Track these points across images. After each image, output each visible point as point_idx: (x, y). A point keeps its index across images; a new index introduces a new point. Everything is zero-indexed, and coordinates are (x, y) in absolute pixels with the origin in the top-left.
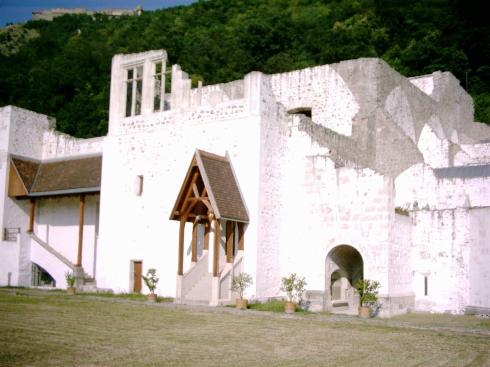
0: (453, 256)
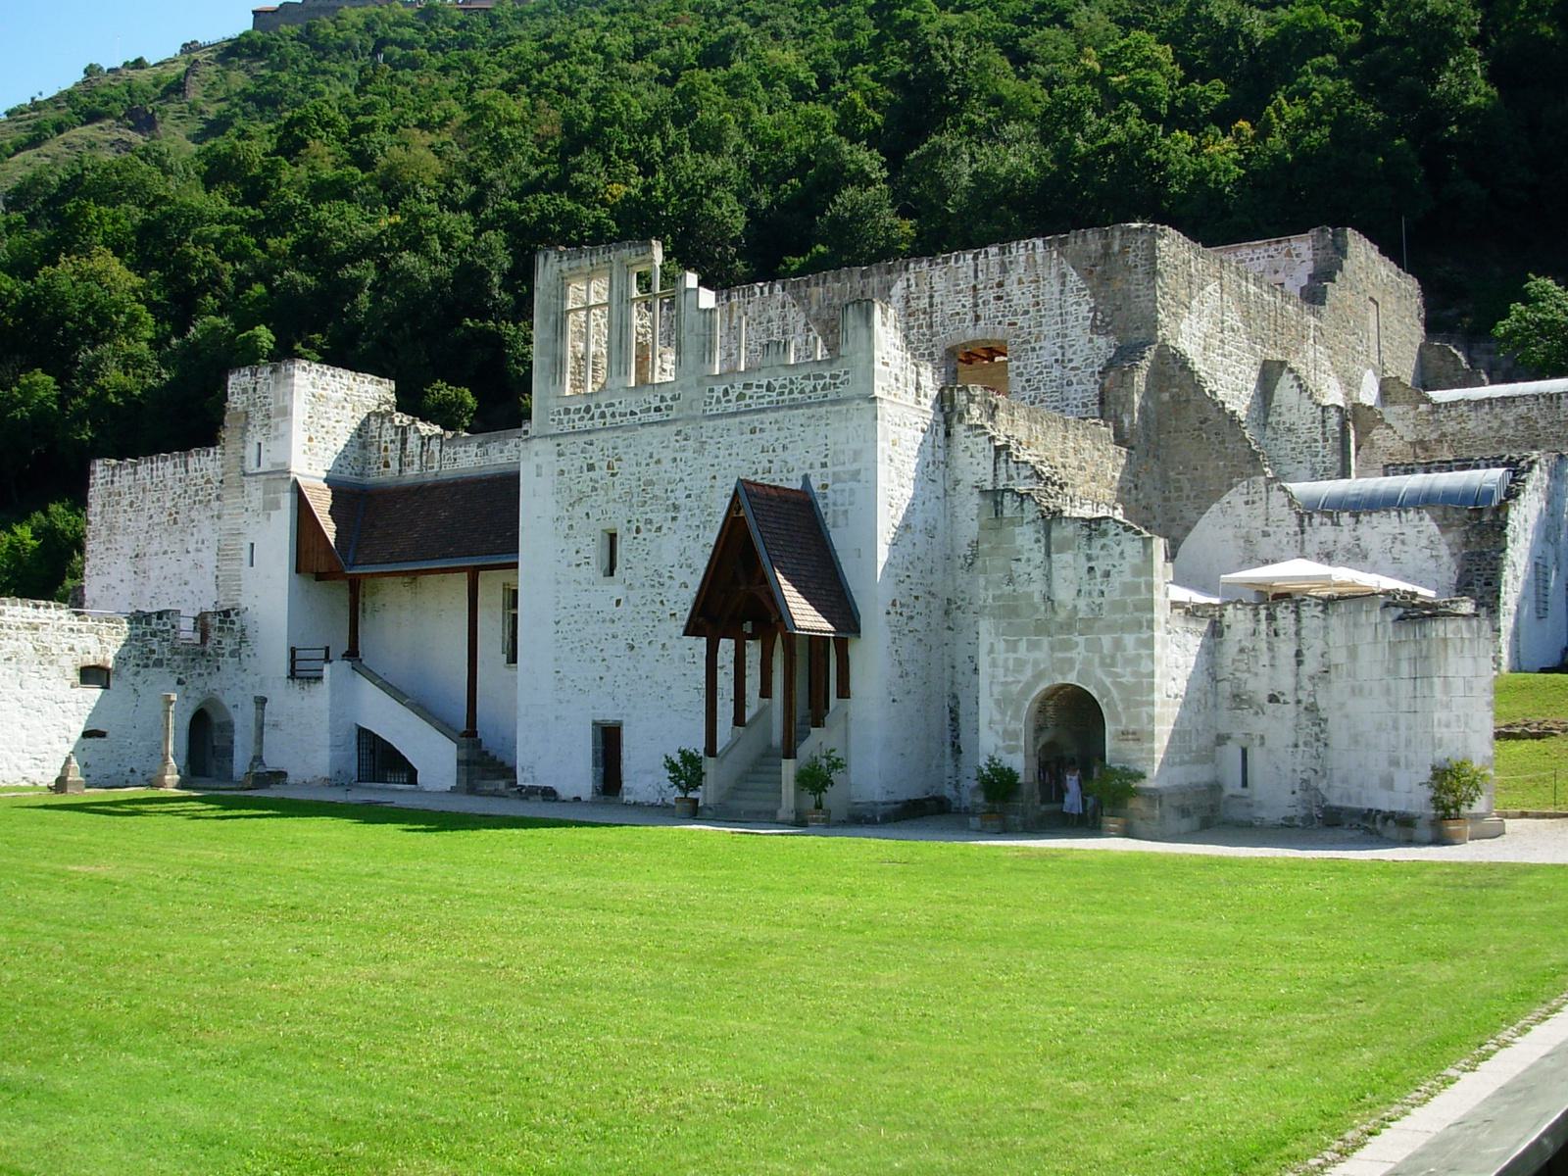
0: (1299, 702)
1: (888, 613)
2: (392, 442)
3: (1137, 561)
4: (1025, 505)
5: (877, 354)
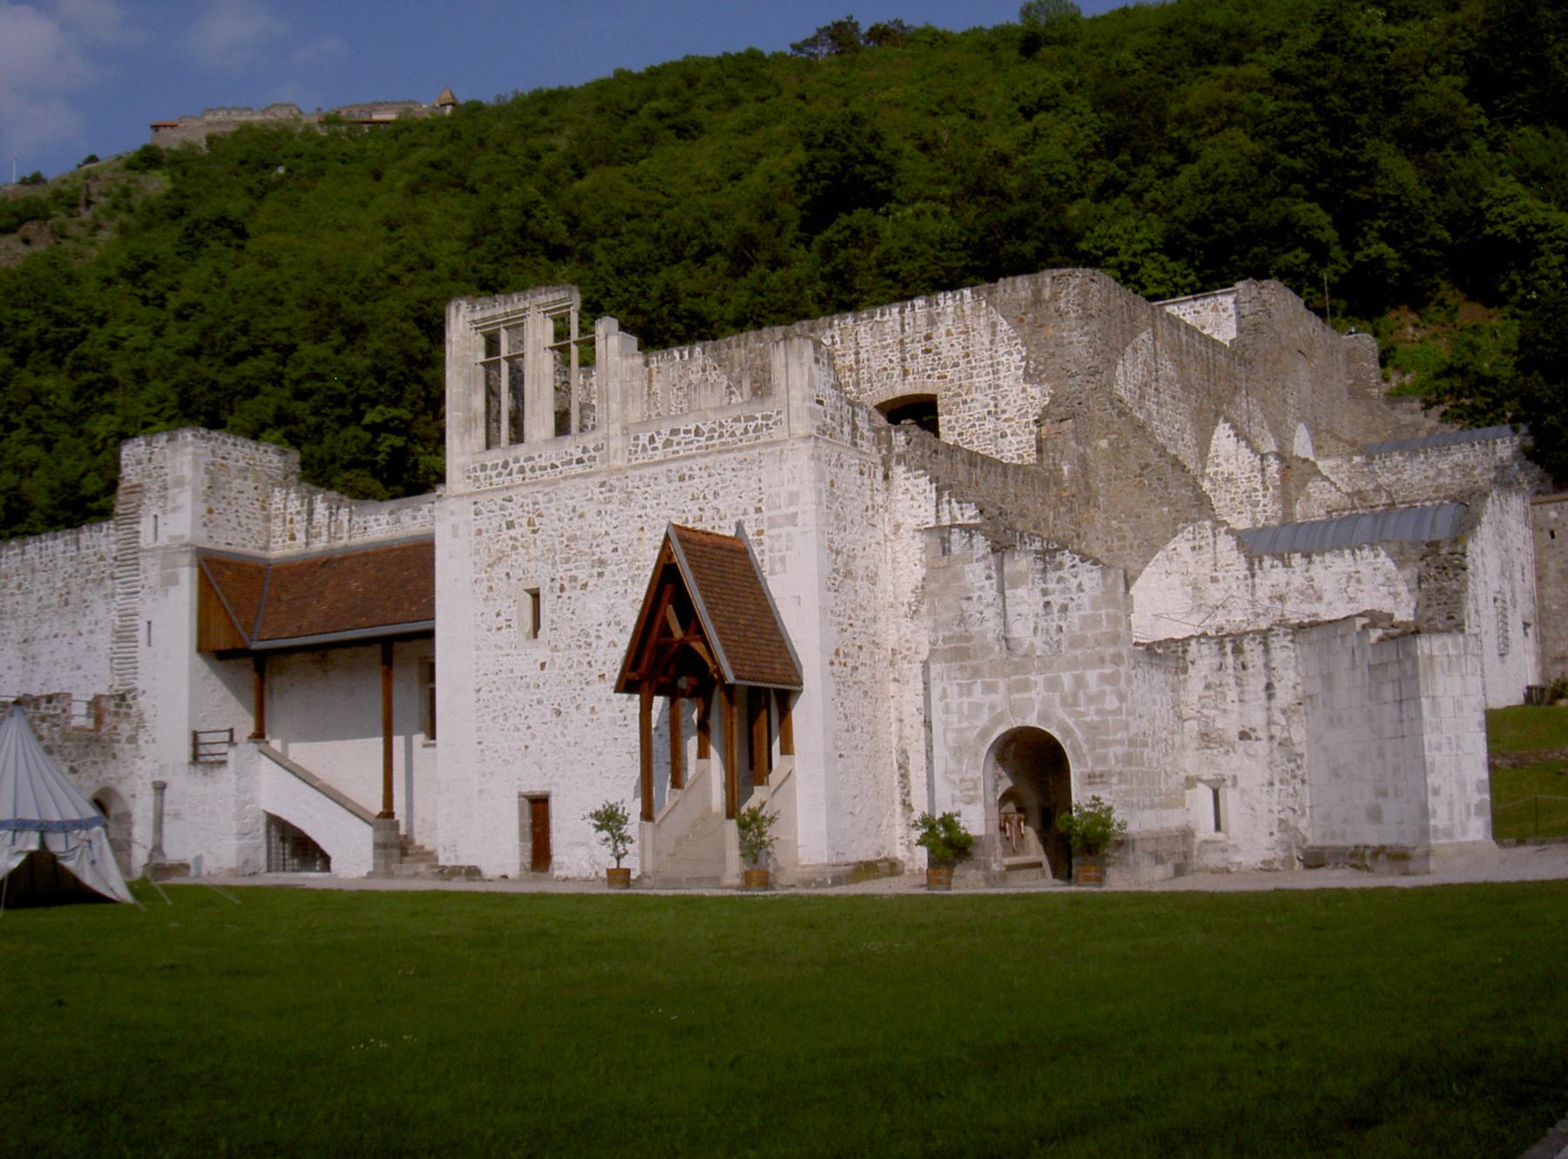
0: (1271, 738)
1: (832, 663)
2: (298, 513)
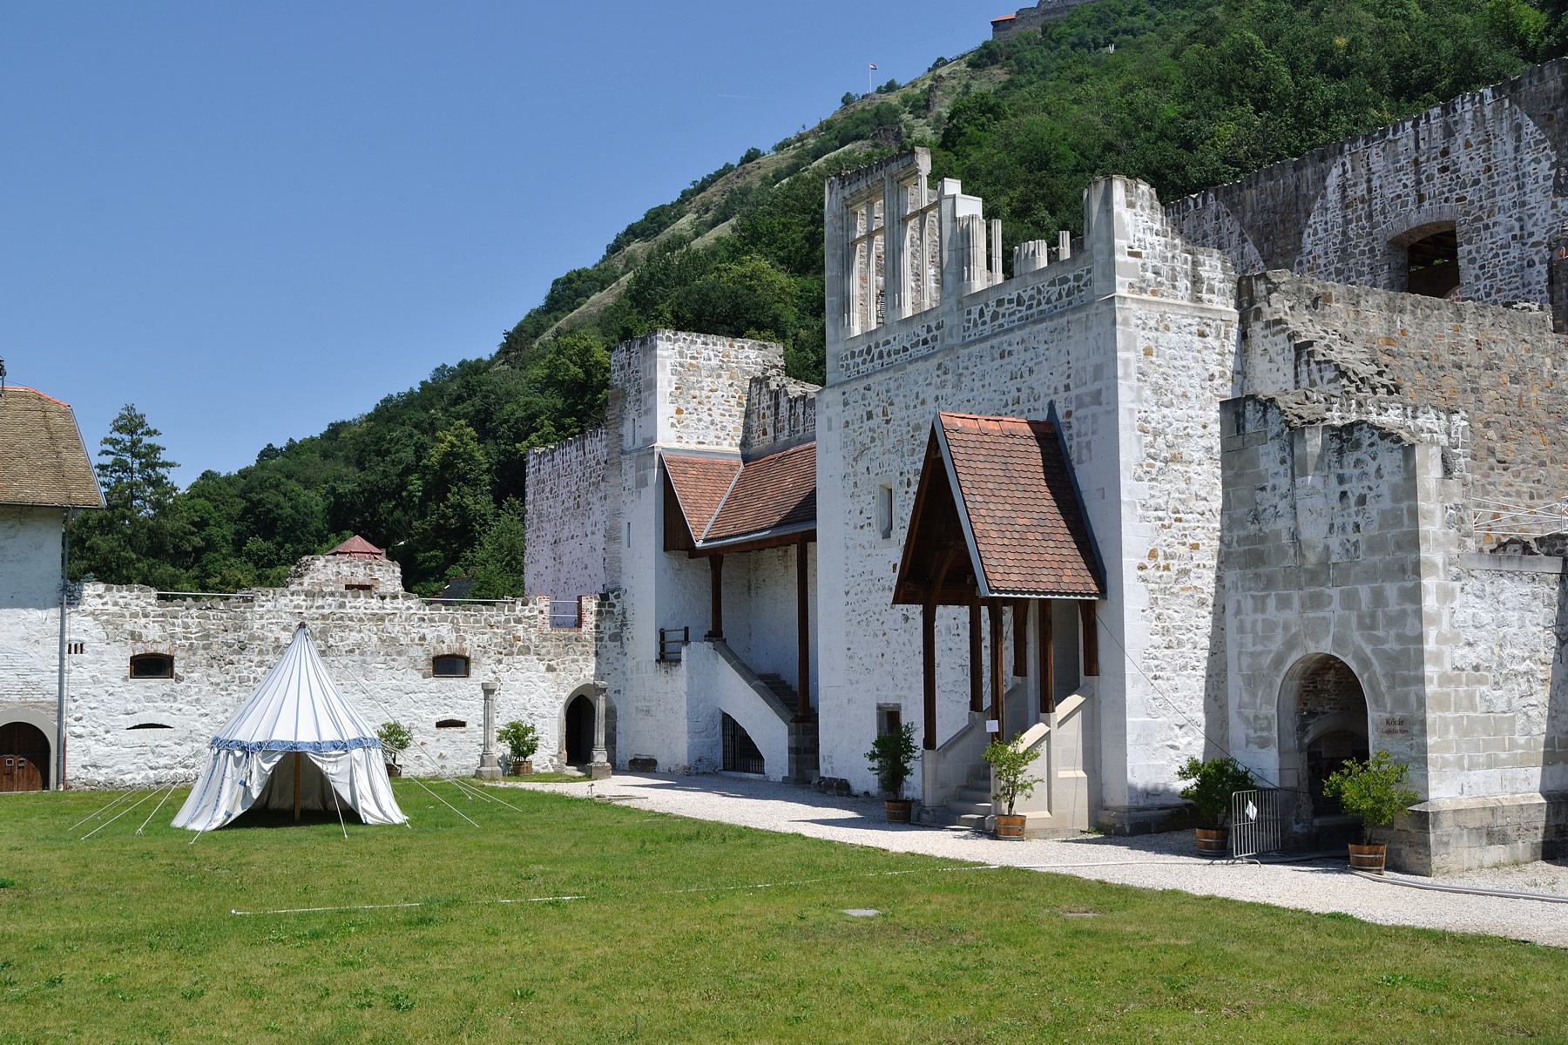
3: (1397, 479)
4: (1269, 415)
5: (1119, 243)
